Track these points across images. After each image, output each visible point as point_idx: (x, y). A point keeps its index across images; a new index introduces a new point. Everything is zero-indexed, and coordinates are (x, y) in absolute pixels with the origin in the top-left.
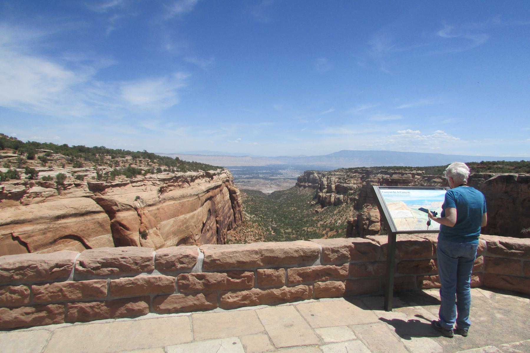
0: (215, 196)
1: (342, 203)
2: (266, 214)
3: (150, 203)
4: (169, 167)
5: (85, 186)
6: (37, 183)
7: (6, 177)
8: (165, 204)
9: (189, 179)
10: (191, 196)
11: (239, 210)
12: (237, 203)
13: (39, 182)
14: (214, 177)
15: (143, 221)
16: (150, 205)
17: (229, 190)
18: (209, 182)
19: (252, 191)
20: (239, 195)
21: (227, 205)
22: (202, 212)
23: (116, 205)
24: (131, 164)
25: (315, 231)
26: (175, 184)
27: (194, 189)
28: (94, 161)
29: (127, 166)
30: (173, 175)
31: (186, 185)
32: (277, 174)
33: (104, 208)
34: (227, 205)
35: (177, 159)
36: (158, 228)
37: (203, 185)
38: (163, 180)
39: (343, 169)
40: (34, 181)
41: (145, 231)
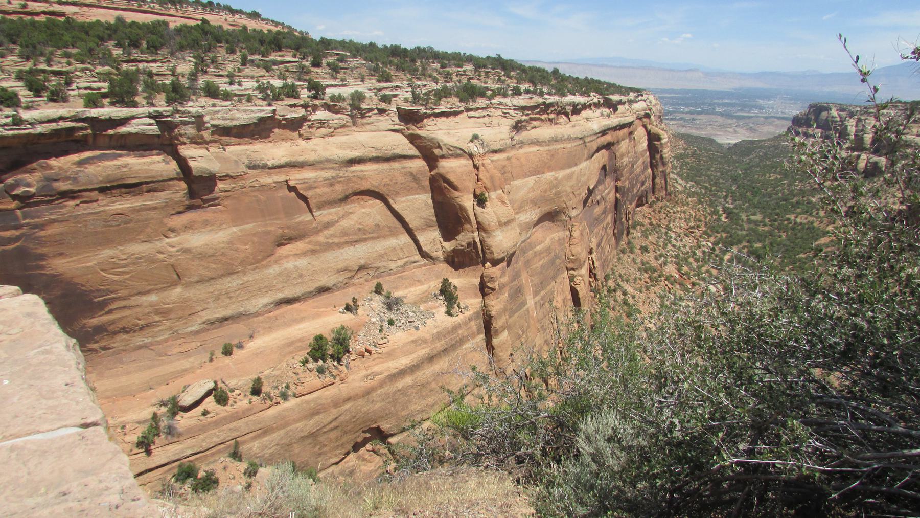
0: (618, 142)
1: (881, 173)
2: (716, 183)
3: (495, 148)
4: (534, 84)
5: (392, 114)
6: (322, 106)
7: (280, 94)
8: (521, 151)
9: (569, 109)
10: (570, 139)
11: (663, 172)
12: (662, 158)
13: (326, 104)
14: (619, 107)
15: (481, 176)
16: (495, 152)
17: (649, 133)
18: (609, 116)
19: (697, 137)
20: (666, 143)
21: (640, 161)
22: (588, 169)
23: (439, 147)
24: (472, 78)
25: (812, 223)
26: (543, 117)
27: (577, 128)
28: (409, 72)
29: (465, 81)
30: (541, 100)
31: (563, 119)
32: (752, 107)
33: (420, 152)
34: (640, 161)
35: (556, 72)
36: (506, 191)
37: (595, 120)
38: (523, 109)
39: (900, 102)
40: (317, 102)
41: (482, 194)
